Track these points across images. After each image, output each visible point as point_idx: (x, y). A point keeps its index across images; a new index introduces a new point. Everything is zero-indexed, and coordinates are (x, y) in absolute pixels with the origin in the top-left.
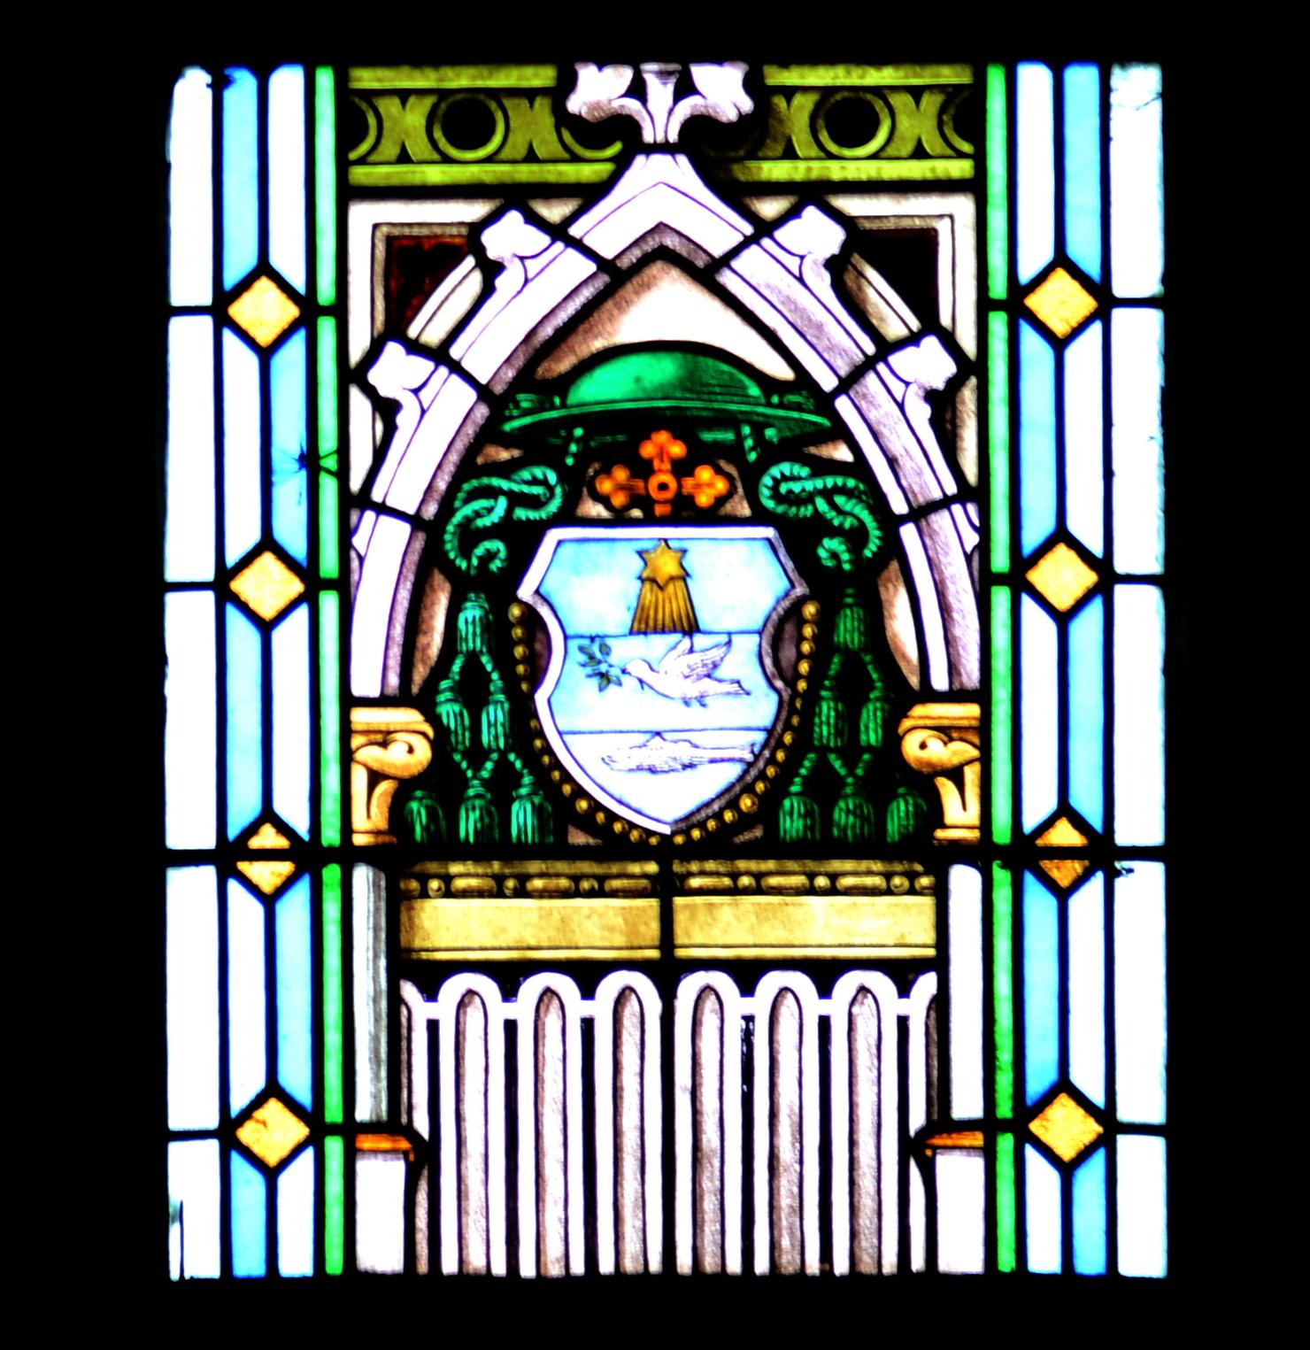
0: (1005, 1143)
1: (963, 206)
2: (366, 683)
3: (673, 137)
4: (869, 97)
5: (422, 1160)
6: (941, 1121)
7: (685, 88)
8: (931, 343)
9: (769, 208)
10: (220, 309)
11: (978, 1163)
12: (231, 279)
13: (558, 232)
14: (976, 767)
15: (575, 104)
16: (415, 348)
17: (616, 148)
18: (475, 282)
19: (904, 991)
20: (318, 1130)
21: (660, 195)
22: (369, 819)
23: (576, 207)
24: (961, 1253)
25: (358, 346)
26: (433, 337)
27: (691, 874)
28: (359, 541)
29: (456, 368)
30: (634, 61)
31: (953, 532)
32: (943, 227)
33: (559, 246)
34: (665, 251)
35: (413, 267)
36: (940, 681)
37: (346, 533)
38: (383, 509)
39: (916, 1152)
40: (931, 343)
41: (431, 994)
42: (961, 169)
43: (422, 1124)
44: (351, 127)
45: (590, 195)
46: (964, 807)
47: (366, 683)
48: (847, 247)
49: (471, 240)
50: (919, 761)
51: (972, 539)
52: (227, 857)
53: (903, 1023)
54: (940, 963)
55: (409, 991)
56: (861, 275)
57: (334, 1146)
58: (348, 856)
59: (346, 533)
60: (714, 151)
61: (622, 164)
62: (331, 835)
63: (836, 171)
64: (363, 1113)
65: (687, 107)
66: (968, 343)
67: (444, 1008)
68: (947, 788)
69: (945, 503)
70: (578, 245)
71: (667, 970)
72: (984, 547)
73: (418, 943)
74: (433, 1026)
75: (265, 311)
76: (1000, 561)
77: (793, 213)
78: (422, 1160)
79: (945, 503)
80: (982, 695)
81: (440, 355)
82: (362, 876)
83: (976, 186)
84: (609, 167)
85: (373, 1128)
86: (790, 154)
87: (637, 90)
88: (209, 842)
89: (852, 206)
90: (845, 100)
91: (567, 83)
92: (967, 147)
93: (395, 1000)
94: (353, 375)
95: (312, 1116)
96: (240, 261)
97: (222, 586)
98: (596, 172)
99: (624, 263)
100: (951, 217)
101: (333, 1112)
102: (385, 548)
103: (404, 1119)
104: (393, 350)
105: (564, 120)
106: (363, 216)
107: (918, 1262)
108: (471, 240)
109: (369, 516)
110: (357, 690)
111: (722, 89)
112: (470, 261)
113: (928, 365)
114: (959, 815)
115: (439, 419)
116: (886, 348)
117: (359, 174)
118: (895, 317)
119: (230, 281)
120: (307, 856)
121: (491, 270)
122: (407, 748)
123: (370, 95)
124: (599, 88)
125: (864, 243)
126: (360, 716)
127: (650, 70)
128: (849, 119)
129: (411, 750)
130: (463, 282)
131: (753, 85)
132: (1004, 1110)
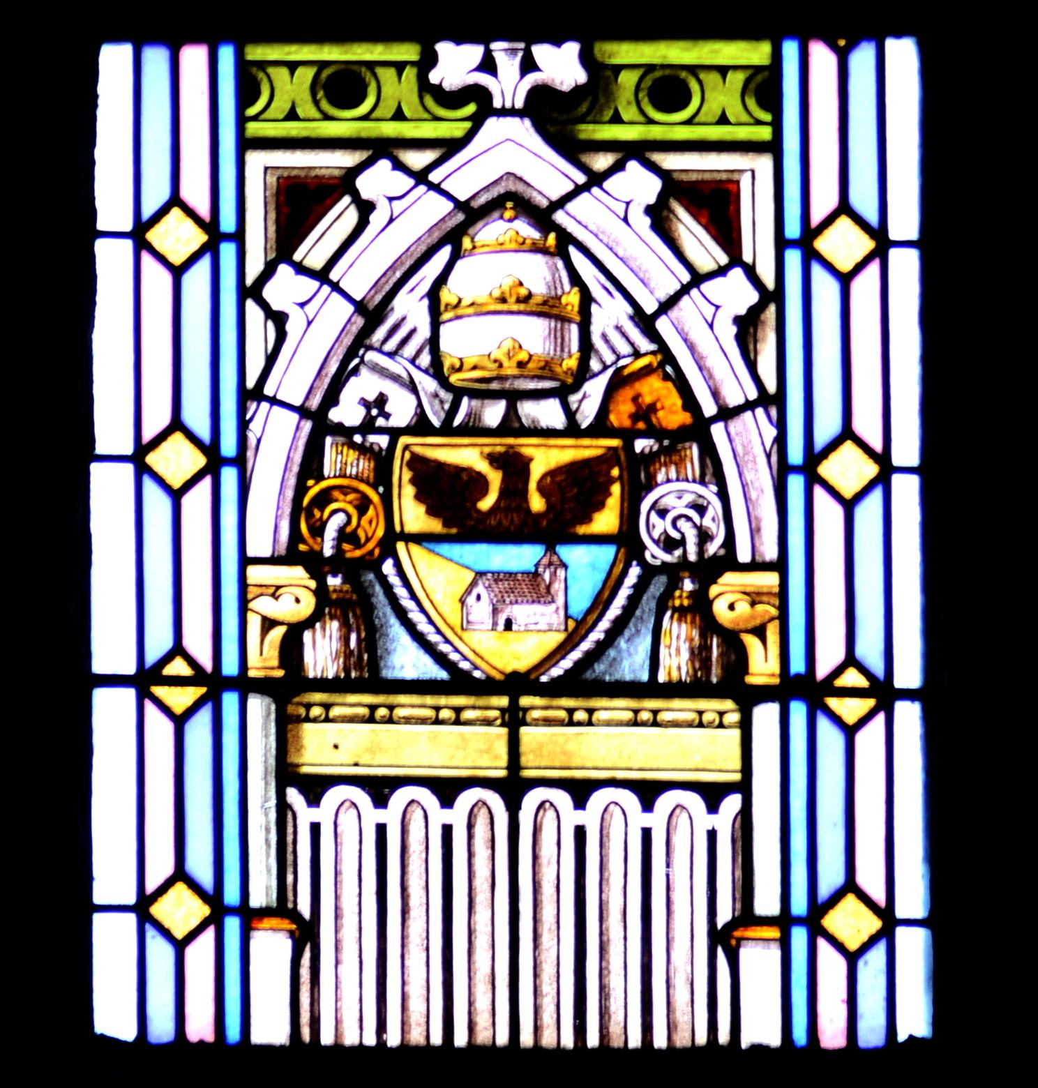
0: (799, 936)
1: (764, 164)
2: (259, 546)
3: (519, 104)
4: (683, 74)
5: (305, 935)
6: (746, 917)
7: (528, 66)
8: (737, 273)
9: (602, 162)
10: (139, 235)
11: (775, 953)
12: (148, 434)
13: (420, 177)
14: (777, 622)
15: (434, 77)
16: (301, 269)
17: (471, 109)
18: (352, 217)
19: (713, 808)
20: (218, 912)
21: (510, 152)
22: (264, 658)
23: (438, 156)
24: (762, 1028)
25: (254, 268)
26: (316, 261)
27: (533, 708)
28: (255, 428)
29: (336, 287)
30: (482, 36)
31: (754, 431)
32: (745, 182)
33: (422, 188)
34: (512, 199)
35: (299, 204)
36: (744, 556)
37: (243, 425)
38: (274, 401)
39: (724, 940)
40: (737, 273)
41: (314, 800)
42: (765, 133)
43: (305, 908)
44: (247, 91)
45: (450, 147)
46: (766, 661)
47: (259, 546)
48: (663, 197)
49: (346, 183)
50: (732, 621)
51: (770, 433)
52: (145, 680)
53: (712, 835)
54: (744, 787)
55: (293, 795)
56: (672, 212)
57: (232, 925)
58: (244, 685)
59: (243, 425)
60: (552, 115)
61: (477, 122)
62: (230, 667)
63: (656, 133)
64: (258, 899)
65: (532, 79)
66: (768, 276)
67: (323, 813)
68: (751, 641)
69: (749, 406)
70: (436, 188)
71: (513, 787)
72: (781, 440)
73: (301, 761)
74: (315, 828)
75: (176, 237)
76: (796, 455)
77: (618, 167)
78: (305, 935)
79: (749, 406)
80: (780, 565)
81: (322, 276)
82: (258, 706)
83: (774, 148)
84: (468, 125)
85: (265, 912)
86: (617, 119)
87: (488, 65)
88: (130, 668)
89: (671, 161)
90: (663, 78)
91: (429, 60)
92: (767, 117)
93: (283, 808)
94: (250, 292)
95: (214, 898)
96: (156, 418)
97: (142, 907)
98: (755, 931)
99: (476, 204)
100: (753, 172)
101: (231, 895)
102: (278, 437)
103: (290, 905)
104: (284, 270)
105: (425, 87)
106: (257, 161)
107: (724, 1037)
108: (346, 183)
109: (265, 405)
110: (251, 552)
111: (561, 65)
112: (347, 199)
113: (735, 294)
114: (762, 666)
115: (322, 326)
116: (698, 279)
117: (253, 129)
118: (703, 249)
119: (150, 887)
120: (213, 684)
121: (366, 208)
122: (293, 599)
123: (263, 65)
124: (456, 63)
125: (675, 188)
126: (255, 574)
127: (497, 46)
128: (668, 90)
129: (298, 601)
130: (342, 217)
131: (587, 59)
132: (799, 906)
